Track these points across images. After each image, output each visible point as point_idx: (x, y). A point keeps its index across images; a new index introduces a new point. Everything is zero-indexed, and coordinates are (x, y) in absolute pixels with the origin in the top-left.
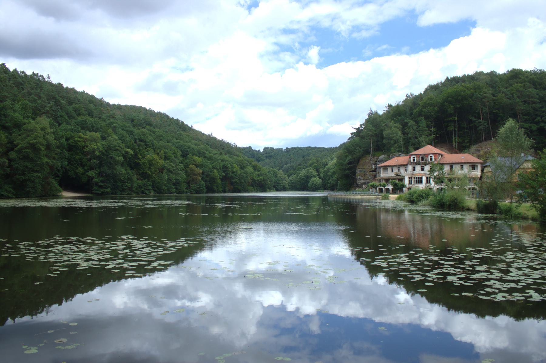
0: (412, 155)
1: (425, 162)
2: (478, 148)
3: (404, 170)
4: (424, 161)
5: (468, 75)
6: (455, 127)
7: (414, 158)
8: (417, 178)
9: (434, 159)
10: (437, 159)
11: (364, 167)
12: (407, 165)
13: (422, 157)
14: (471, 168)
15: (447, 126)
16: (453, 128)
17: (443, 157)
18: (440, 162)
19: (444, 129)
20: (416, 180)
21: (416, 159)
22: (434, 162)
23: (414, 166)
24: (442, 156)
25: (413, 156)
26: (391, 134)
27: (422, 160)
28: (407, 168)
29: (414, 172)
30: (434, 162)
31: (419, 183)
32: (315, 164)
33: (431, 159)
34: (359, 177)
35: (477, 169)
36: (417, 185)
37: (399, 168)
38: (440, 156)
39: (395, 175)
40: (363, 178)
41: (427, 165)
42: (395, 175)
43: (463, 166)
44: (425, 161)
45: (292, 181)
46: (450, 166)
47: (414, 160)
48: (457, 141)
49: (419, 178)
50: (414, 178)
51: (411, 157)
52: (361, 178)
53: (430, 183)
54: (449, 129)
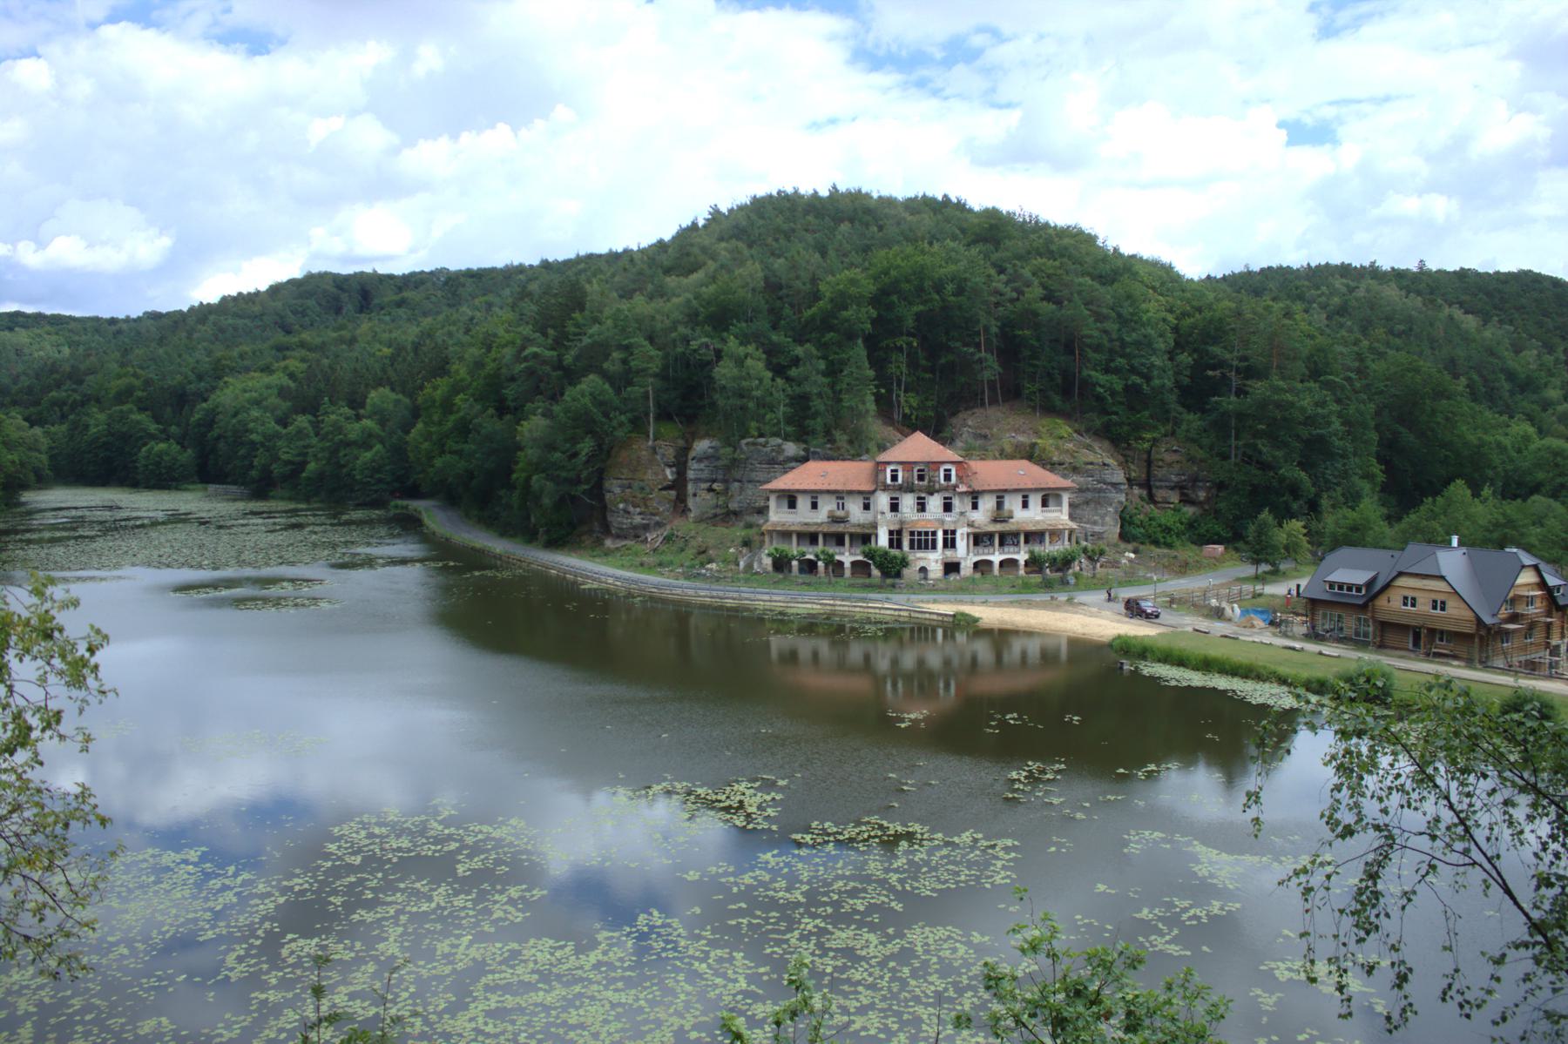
0: (889, 463)
3: (809, 505)
4: (926, 483)
5: (924, 196)
20: (919, 541)
21: (900, 475)
25: (893, 467)
27: (921, 478)
28: (871, 501)
31: (926, 548)
32: (140, 394)
33: (948, 477)
36: (920, 554)
40: (638, 510)
44: (930, 481)
47: (894, 478)
49: (926, 533)
50: (912, 533)
52: (631, 509)
53: (953, 545)
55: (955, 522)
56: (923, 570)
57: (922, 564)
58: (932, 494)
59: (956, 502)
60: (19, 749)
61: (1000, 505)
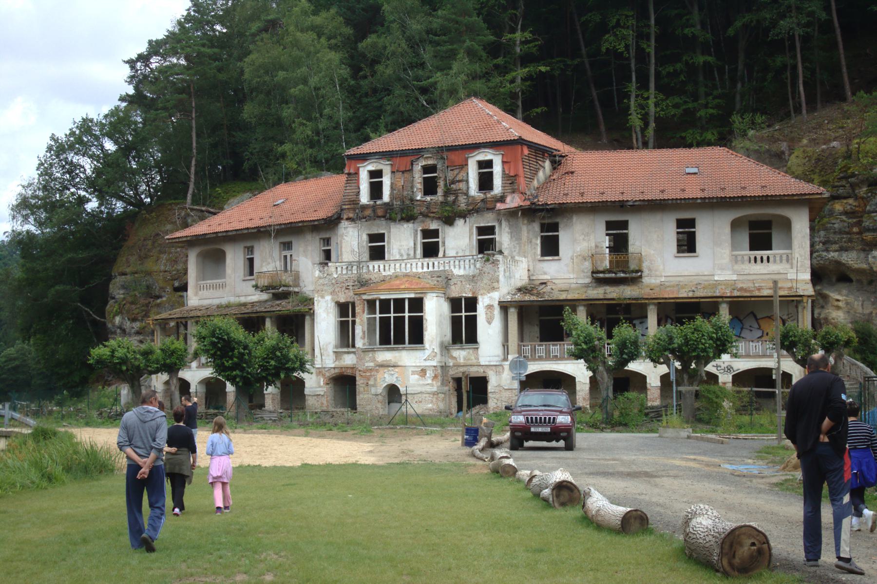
0: (364, 157)
1: (444, 203)
2: (773, 140)
3: (318, 257)
4: (439, 197)
6: (642, 36)
7: (376, 174)
8: (385, 305)
9: (505, 176)
10: (522, 180)
11: (150, 265)
12: (331, 224)
13: (426, 169)
14: (745, 239)
15: (603, 29)
16: (631, 41)
17: (562, 170)
18: (542, 200)
19: (584, 51)
20: (385, 322)
21: (386, 181)
22: (502, 199)
23: (378, 228)
24: (556, 164)
26: (282, 68)
27: (430, 187)
28: (333, 248)
29: (376, 264)
30: (502, 199)
31: (399, 340)
33: (486, 182)
34: (117, 320)
35: (789, 246)
36: (385, 356)
37: (288, 246)
38: (547, 164)
39: (264, 296)
40: (137, 325)
41: (460, 222)
42: (264, 296)
43: (691, 223)
44: (447, 193)
45: (17, 363)
46: (610, 225)
47: (376, 190)
48: (652, 109)
51: (357, 173)
52: (128, 325)
53: (472, 338)
54: (608, 42)
55: (473, 279)
56: (393, 393)
57: (388, 378)
58: (449, 221)
59: (503, 238)
60: (590, 374)
61: (619, 244)
